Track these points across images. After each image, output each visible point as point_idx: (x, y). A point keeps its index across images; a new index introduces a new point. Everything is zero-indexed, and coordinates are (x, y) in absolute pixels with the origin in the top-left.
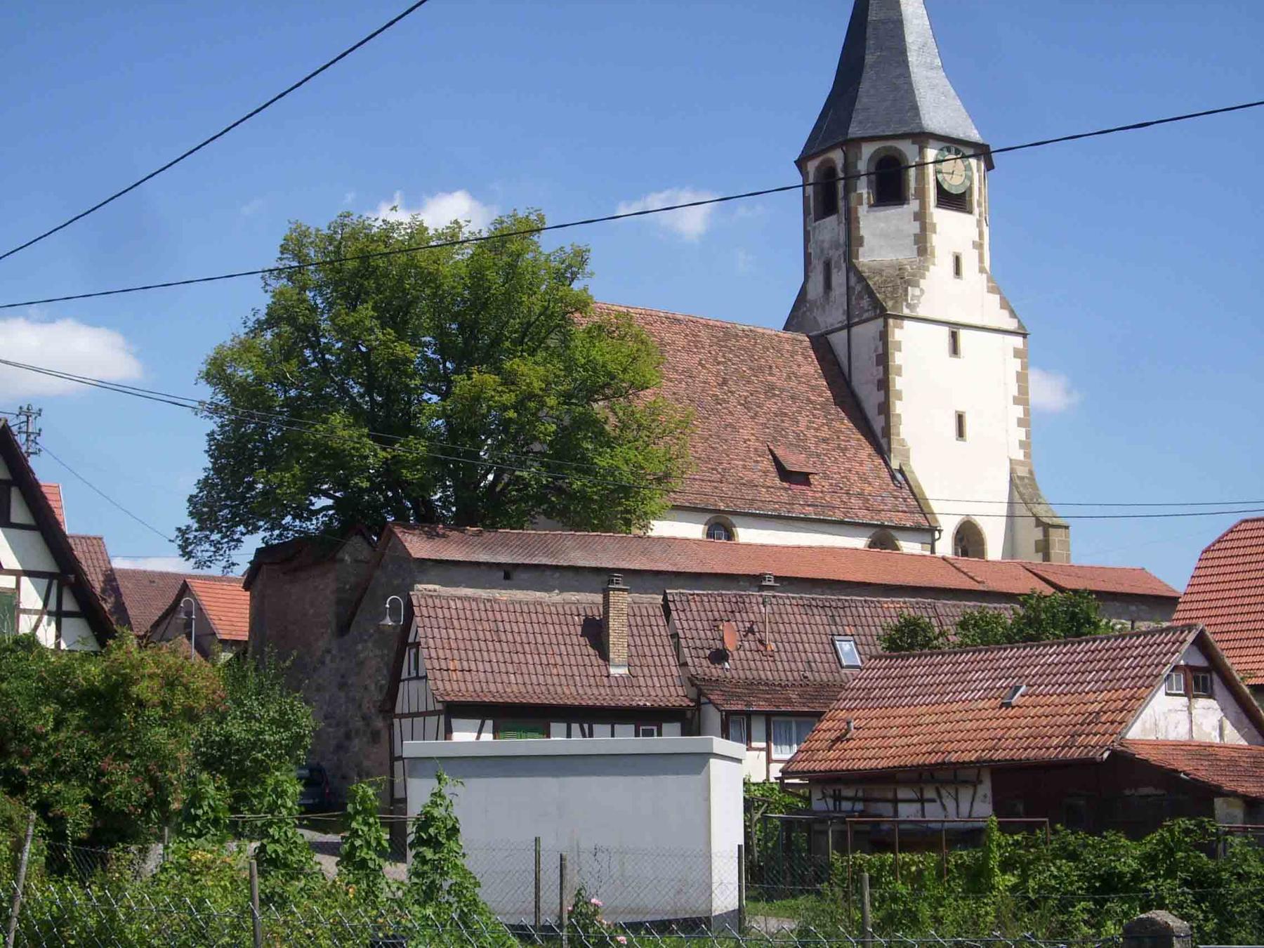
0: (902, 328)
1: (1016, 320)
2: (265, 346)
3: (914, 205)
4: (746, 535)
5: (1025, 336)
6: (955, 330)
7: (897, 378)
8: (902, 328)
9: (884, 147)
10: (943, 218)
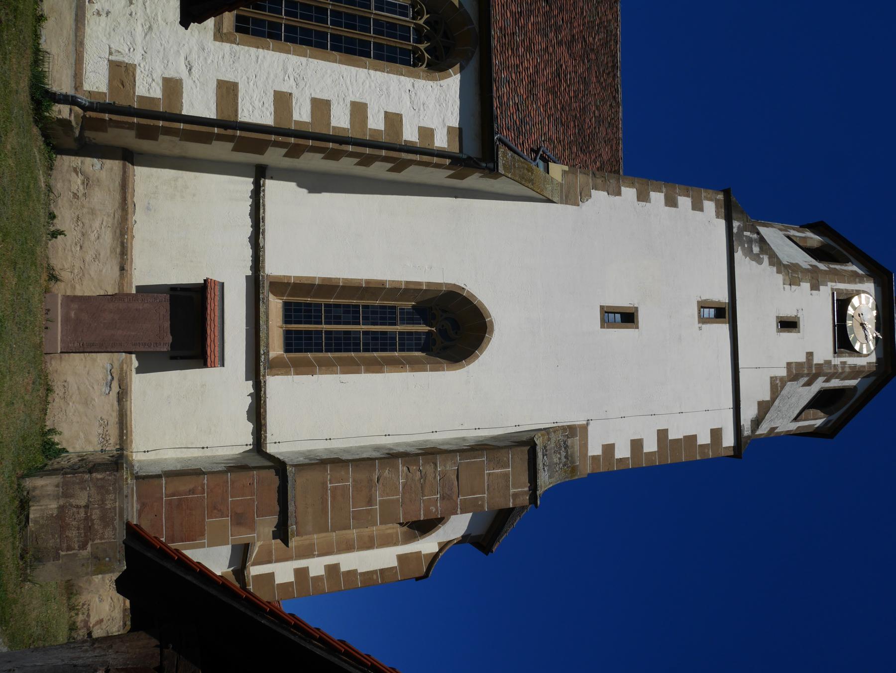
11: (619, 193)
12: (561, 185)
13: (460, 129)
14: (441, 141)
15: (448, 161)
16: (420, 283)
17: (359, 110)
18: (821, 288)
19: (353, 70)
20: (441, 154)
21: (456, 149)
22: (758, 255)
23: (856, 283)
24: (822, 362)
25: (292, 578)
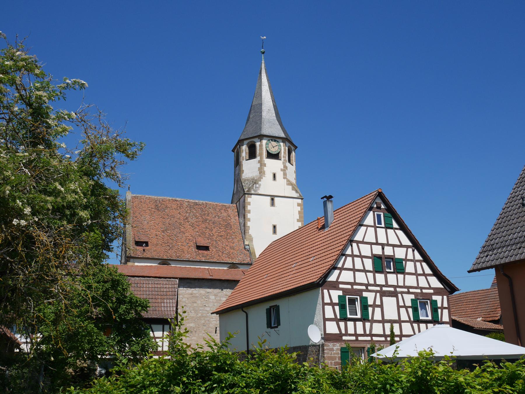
0: (251, 197)
3: (258, 158)
5: (302, 199)
6: (272, 199)
7: (249, 214)
8: (251, 197)
9: (250, 141)
10: (270, 162)
11: (249, 227)
18: (265, 163)
22: (259, 185)
23: (263, 148)
24: (283, 165)
25: (300, 207)
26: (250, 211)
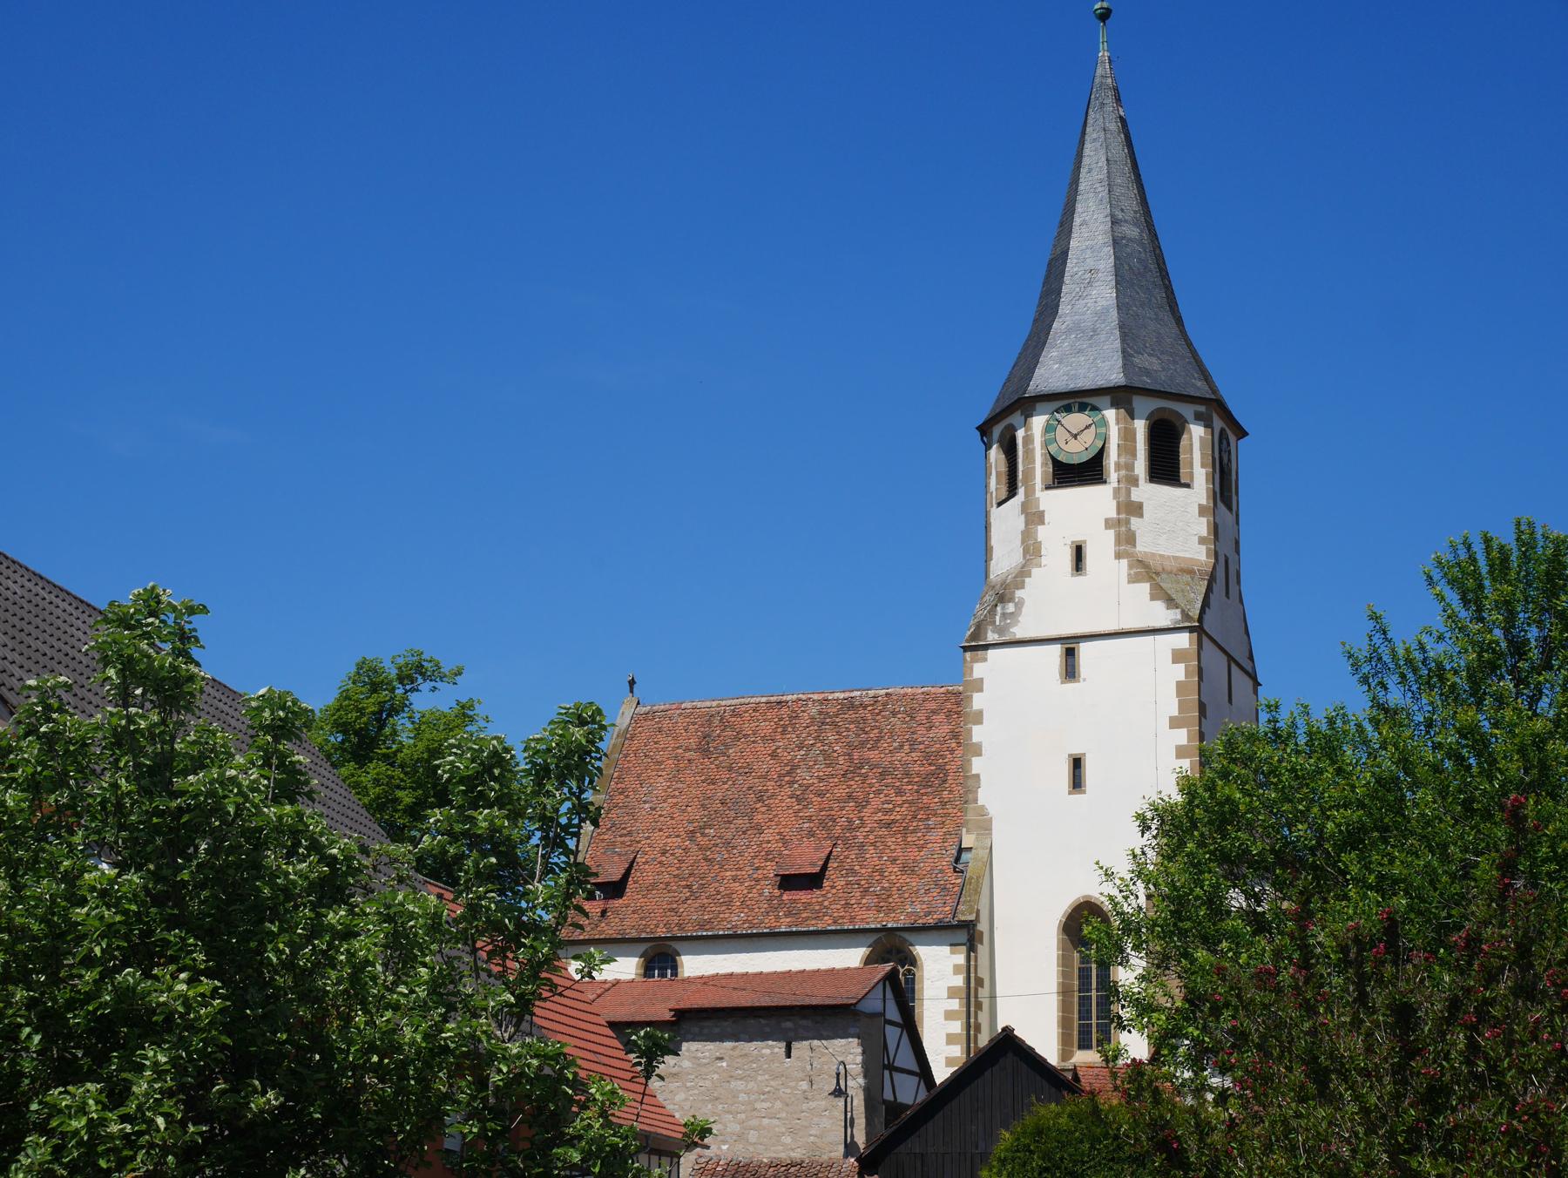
1: (1178, 611)
2: (1141, 958)
4: (694, 965)
11: (978, 776)
12: (978, 834)
13: (951, 945)
14: (960, 959)
15: (972, 954)
16: (1058, 955)
17: (949, 1015)
19: (925, 1019)
20: (968, 959)
21: (964, 948)
22: (1016, 605)
23: (1034, 449)
26: (980, 713)
